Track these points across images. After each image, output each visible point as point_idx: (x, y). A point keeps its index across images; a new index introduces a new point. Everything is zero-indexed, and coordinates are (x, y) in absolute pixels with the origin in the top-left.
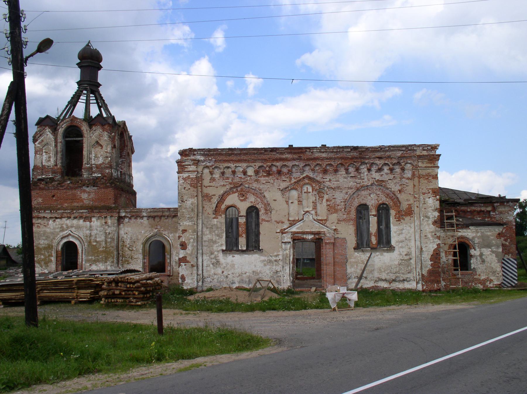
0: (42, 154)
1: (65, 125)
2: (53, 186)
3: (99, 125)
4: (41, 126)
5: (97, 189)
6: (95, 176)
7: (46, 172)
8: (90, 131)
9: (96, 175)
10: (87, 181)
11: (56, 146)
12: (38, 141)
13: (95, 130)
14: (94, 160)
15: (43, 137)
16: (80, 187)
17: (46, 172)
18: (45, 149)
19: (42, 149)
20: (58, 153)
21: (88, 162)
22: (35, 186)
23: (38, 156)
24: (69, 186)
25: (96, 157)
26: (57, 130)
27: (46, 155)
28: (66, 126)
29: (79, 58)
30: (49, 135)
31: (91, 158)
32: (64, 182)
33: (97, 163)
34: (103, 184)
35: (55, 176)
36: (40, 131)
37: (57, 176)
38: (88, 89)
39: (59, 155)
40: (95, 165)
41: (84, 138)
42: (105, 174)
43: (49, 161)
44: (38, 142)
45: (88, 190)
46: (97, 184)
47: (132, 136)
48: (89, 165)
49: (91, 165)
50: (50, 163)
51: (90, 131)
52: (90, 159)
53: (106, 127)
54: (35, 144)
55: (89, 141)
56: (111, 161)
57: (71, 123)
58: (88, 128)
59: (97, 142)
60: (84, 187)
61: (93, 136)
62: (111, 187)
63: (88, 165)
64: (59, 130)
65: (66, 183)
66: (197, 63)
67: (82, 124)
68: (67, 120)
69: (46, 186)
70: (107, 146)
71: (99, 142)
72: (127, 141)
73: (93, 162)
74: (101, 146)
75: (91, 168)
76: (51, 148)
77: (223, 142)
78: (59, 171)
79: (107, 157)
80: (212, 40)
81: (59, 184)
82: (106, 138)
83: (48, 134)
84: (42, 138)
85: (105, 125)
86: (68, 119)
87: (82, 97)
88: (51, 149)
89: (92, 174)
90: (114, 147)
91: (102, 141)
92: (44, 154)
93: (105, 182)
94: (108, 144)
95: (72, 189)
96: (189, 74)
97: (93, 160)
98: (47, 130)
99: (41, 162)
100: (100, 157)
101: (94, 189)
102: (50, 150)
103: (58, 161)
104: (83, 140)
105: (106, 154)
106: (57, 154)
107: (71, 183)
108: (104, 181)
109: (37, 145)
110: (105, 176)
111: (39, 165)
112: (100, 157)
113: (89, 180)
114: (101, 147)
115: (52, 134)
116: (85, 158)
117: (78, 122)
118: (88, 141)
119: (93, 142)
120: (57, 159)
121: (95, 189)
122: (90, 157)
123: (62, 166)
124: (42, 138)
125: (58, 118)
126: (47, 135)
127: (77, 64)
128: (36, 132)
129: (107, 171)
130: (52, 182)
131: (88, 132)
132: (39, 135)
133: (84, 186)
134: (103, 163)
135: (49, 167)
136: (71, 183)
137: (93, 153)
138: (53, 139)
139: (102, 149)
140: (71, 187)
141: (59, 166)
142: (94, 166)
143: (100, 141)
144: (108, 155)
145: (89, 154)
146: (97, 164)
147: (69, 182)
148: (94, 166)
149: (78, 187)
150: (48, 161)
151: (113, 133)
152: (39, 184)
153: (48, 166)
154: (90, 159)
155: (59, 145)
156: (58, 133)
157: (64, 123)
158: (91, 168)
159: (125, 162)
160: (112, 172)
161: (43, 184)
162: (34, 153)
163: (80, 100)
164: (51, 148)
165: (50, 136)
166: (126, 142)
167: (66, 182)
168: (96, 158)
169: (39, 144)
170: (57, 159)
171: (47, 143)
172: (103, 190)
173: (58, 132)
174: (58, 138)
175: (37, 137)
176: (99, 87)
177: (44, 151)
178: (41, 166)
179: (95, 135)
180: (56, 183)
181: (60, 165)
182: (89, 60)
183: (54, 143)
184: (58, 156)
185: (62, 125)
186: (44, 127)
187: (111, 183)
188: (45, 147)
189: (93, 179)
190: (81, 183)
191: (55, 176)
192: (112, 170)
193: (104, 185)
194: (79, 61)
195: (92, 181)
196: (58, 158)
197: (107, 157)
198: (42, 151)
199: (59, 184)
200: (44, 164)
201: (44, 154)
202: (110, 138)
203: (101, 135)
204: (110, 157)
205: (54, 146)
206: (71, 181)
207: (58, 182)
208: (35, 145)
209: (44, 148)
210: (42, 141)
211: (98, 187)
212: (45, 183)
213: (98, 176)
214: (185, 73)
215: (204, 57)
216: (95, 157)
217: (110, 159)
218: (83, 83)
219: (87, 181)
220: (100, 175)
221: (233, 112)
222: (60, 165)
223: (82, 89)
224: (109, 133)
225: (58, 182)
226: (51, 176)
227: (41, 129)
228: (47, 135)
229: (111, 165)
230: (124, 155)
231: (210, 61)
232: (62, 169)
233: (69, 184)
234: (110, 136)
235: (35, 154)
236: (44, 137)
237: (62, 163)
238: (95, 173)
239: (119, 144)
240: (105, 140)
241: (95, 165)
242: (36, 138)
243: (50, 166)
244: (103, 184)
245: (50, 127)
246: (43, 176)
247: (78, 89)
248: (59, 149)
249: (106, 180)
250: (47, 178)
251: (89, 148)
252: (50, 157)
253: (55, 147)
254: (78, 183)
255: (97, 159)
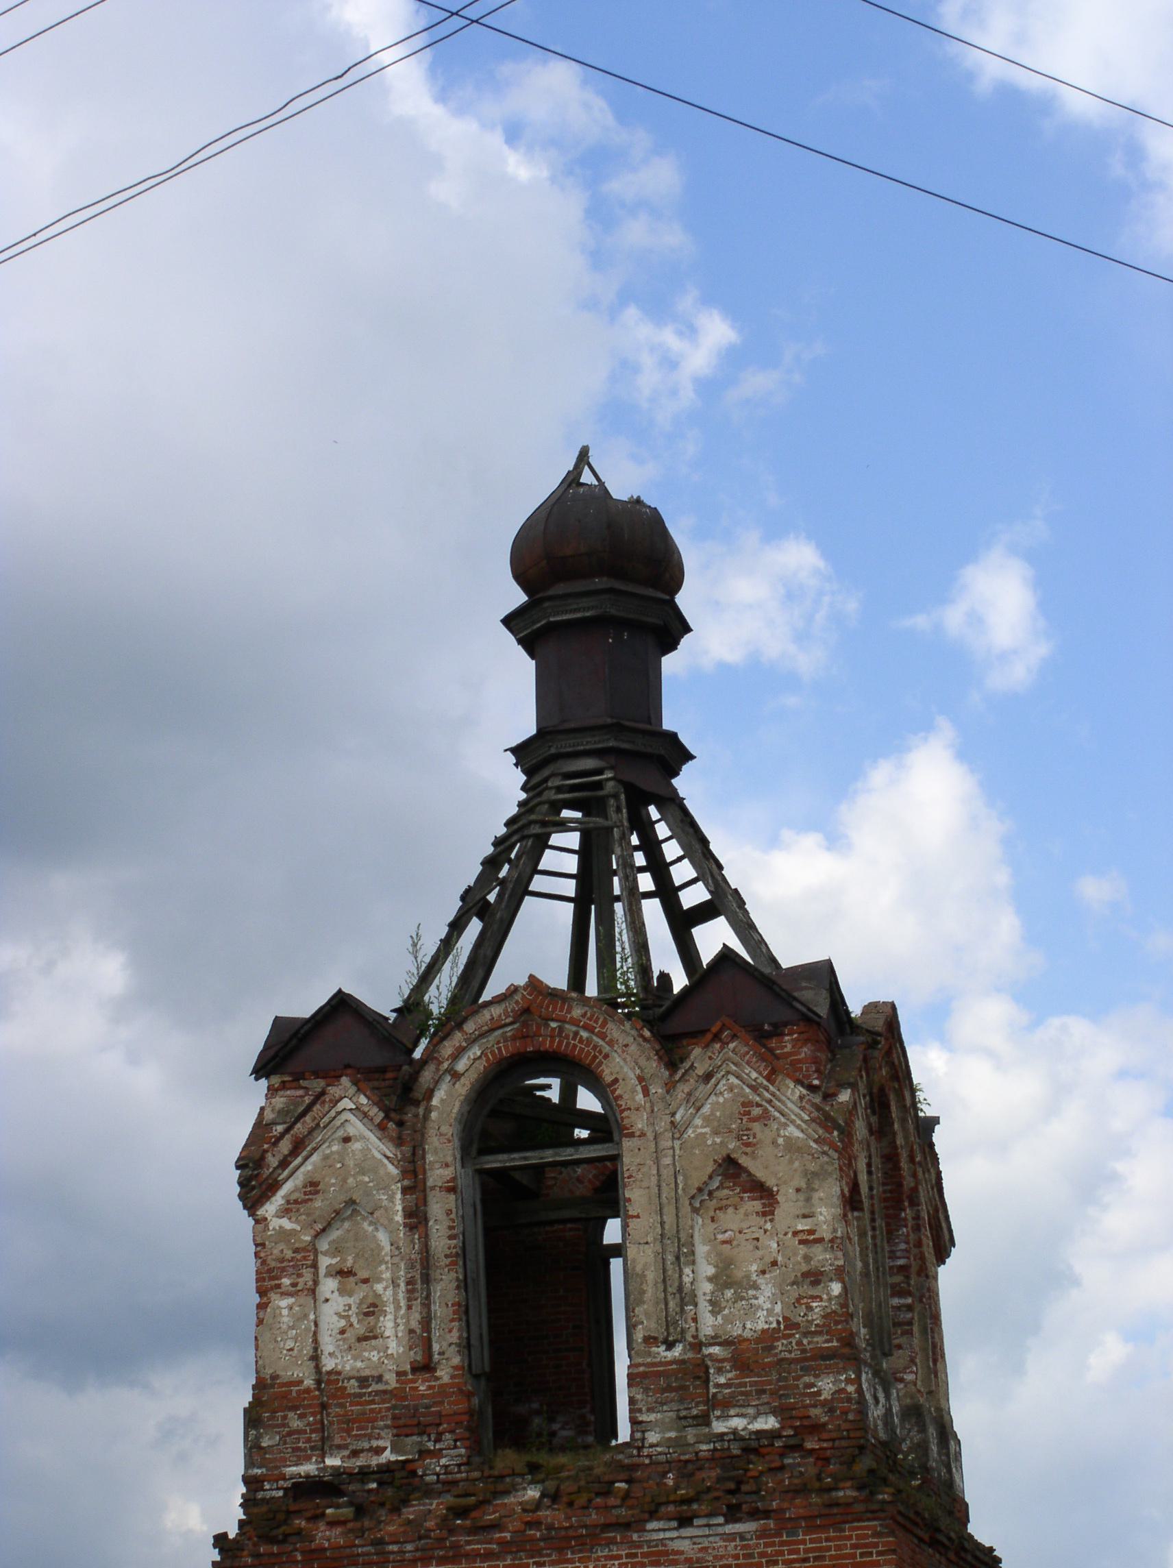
0: (313, 1292)
1: (476, 1051)
2: (415, 1530)
3: (734, 1037)
4: (298, 1077)
5: (762, 1534)
6: (735, 1432)
7: (348, 1423)
8: (670, 1087)
9: (738, 1423)
10: (670, 1480)
11: (417, 1218)
12: (282, 1192)
13: (708, 1077)
14: (716, 1307)
15: (315, 1158)
16: (627, 1526)
17: (348, 1423)
18: (336, 1250)
19: (316, 1252)
20: (436, 1274)
21: (669, 1323)
22: (273, 1540)
23: (285, 1303)
24: (535, 1524)
25: (727, 1285)
26: (418, 1094)
27: (342, 1291)
28: (481, 1065)
29: (521, 576)
30: (362, 1138)
31: (694, 1295)
32: (497, 1494)
33: (736, 1331)
34: (801, 1490)
35: (424, 1453)
36: (292, 1117)
37: (437, 1454)
38: (610, 787)
39: (445, 1288)
40: (726, 1343)
41: (627, 1144)
42: (815, 1412)
43: (370, 1336)
44: (278, 1200)
45: (684, 1545)
46: (757, 1492)
47: (936, 1121)
48: (677, 1351)
49: (697, 1346)
50: (375, 1356)
51: (670, 1087)
52: (682, 1304)
53: (787, 1044)
54: (260, 1212)
55: (667, 1161)
56: (844, 1305)
57: (522, 1036)
58: (653, 1066)
59: (730, 1168)
60: (651, 1525)
61: (698, 1121)
62: (873, 1514)
63: (670, 1346)
64: (430, 1094)
65: (510, 1500)
66: (879, 775)
67: (603, 1036)
68: (486, 1015)
69: (361, 1533)
70: (811, 1189)
71: (743, 1161)
72: (912, 1159)
73: (708, 1324)
74: (763, 1192)
75: (698, 1371)
76: (383, 1237)
77: (1075, 1282)
78: (447, 1408)
79: (815, 1277)
80: (954, 618)
81: (462, 1512)
82: (793, 1131)
83: (351, 1131)
84: (308, 1167)
85: (778, 1031)
86: (496, 1011)
87: (549, 860)
88: (380, 1248)
89: (704, 1420)
90: (852, 1201)
91: (766, 1152)
92: (329, 1286)
93: (819, 1478)
94: (815, 1174)
95: (561, 1550)
96: (835, 841)
97: (704, 1307)
98: (346, 1103)
99: (308, 1350)
100: (761, 1281)
101: (730, 1537)
102: (375, 1258)
103: (435, 1334)
104: (616, 1158)
105: (802, 1250)
106: (427, 1279)
107: (553, 1497)
108: (809, 1467)
109: (275, 1223)
110: (816, 1428)
111: (297, 1373)
112: (761, 1281)
113: (687, 1468)
114: (757, 1205)
115: (381, 1127)
116: (649, 1295)
117: (575, 1022)
118: (657, 1161)
119: (701, 1169)
120: (426, 1322)
121: (742, 1536)
122: (680, 1289)
123: (469, 1369)
124: (308, 1166)
125: (412, 1007)
126: (347, 1140)
127: (508, 621)
128: (261, 1127)
129: (826, 1386)
130: (405, 1502)
131: (657, 1089)
132: (285, 1146)
133: (653, 1515)
134: (790, 1325)
135: (375, 1387)
136: (553, 1497)
137: (701, 1249)
138: (393, 1170)
139: (768, 1212)
140: (550, 1527)
141: (444, 1374)
142: (715, 1350)
143: (754, 1156)
144: (822, 1257)
145: (670, 1258)
146: (741, 1340)
147: (533, 1493)
148: (715, 1350)
149: (607, 1527)
150: (361, 1339)
151: (842, 1085)
152: (300, 1523)
153: (363, 1381)
154: (686, 1297)
155: (440, 1207)
156: (426, 1117)
157: (472, 1041)
158: (698, 1371)
159: (910, 1323)
160: (860, 1391)
161: (332, 1524)
162: (253, 1285)
163: (538, 883)
164: (383, 1237)
165: (366, 1151)
166: (904, 1164)
167: (507, 1493)
168: (729, 1293)
169: (285, 1212)
170: (426, 1322)
171: (351, 1202)
172: (807, 1541)
173: (428, 1110)
174: (430, 1158)
175: (272, 1161)
176: (676, 773)
177: (325, 1262)
178: (309, 1383)
179: (706, 1109)
180: (436, 1505)
181: (456, 1360)
182: (599, 583)
183: (399, 1196)
184: (437, 1290)
185: (456, 1057)
186: (317, 1084)
187: (869, 1484)
188: (335, 1234)
189: (720, 1458)
190: (627, 1495)
191: (424, 1453)
192: (859, 1377)
193: (814, 1499)
194: (518, 597)
195: (710, 1475)
196: (437, 1309)
197: (815, 1277)
198: (315, 1266)
199: (462, 1512)
200: (329, 1364)
201: (329, 1286)
202: (828, 1130)
203: (756, 1111)
204: (840, 1274)
205: (399, 1218)
206: (551, 1485)
207: (449, 1499)
208: (260, 1221)
209: (323, 1245)
210: (313, 1187)
211: (766, 1514)
212: (348, 1512)
213: (759, 1433)
214: (811, 841)
215: (926, 727)
216: (724, 1278)
217: (836, 1288)
218: (566, 745)
219: (670, 1480)
220: (769, 1423)
221: (1123, 1074)
222: (456, 1360)
223: (559, 789)
224: (812, 1088)
225: (449, 1499)
226: (388, 1456)
227: (294, 1102)
228: (347, 1140)
229: (848, 1341)
230: (902, 1269)
231: (965, 753)
232: (469, 1395)
233: (538, 1505)
234: (827, 1117)
235: (262, 1292)
236: (326, 1158)
237: (466, 1346)
238: (726, 1405)
239: (878, 1175)
240: (792, 1147)
241: (726, 1343)
242: (266, 1172)
243: (379, 1379)
244: (801, 1490)
245: (366, 1076)
246: (330, 1462)
247: (523, 796)
248: (441, 1240)
249: (822, 1459)
250: (364, 1474)
251: (669, 1219)
252: (372, 1310)
253: (411, 1228)
254: (607, 1493)
255: (738, 1298)
